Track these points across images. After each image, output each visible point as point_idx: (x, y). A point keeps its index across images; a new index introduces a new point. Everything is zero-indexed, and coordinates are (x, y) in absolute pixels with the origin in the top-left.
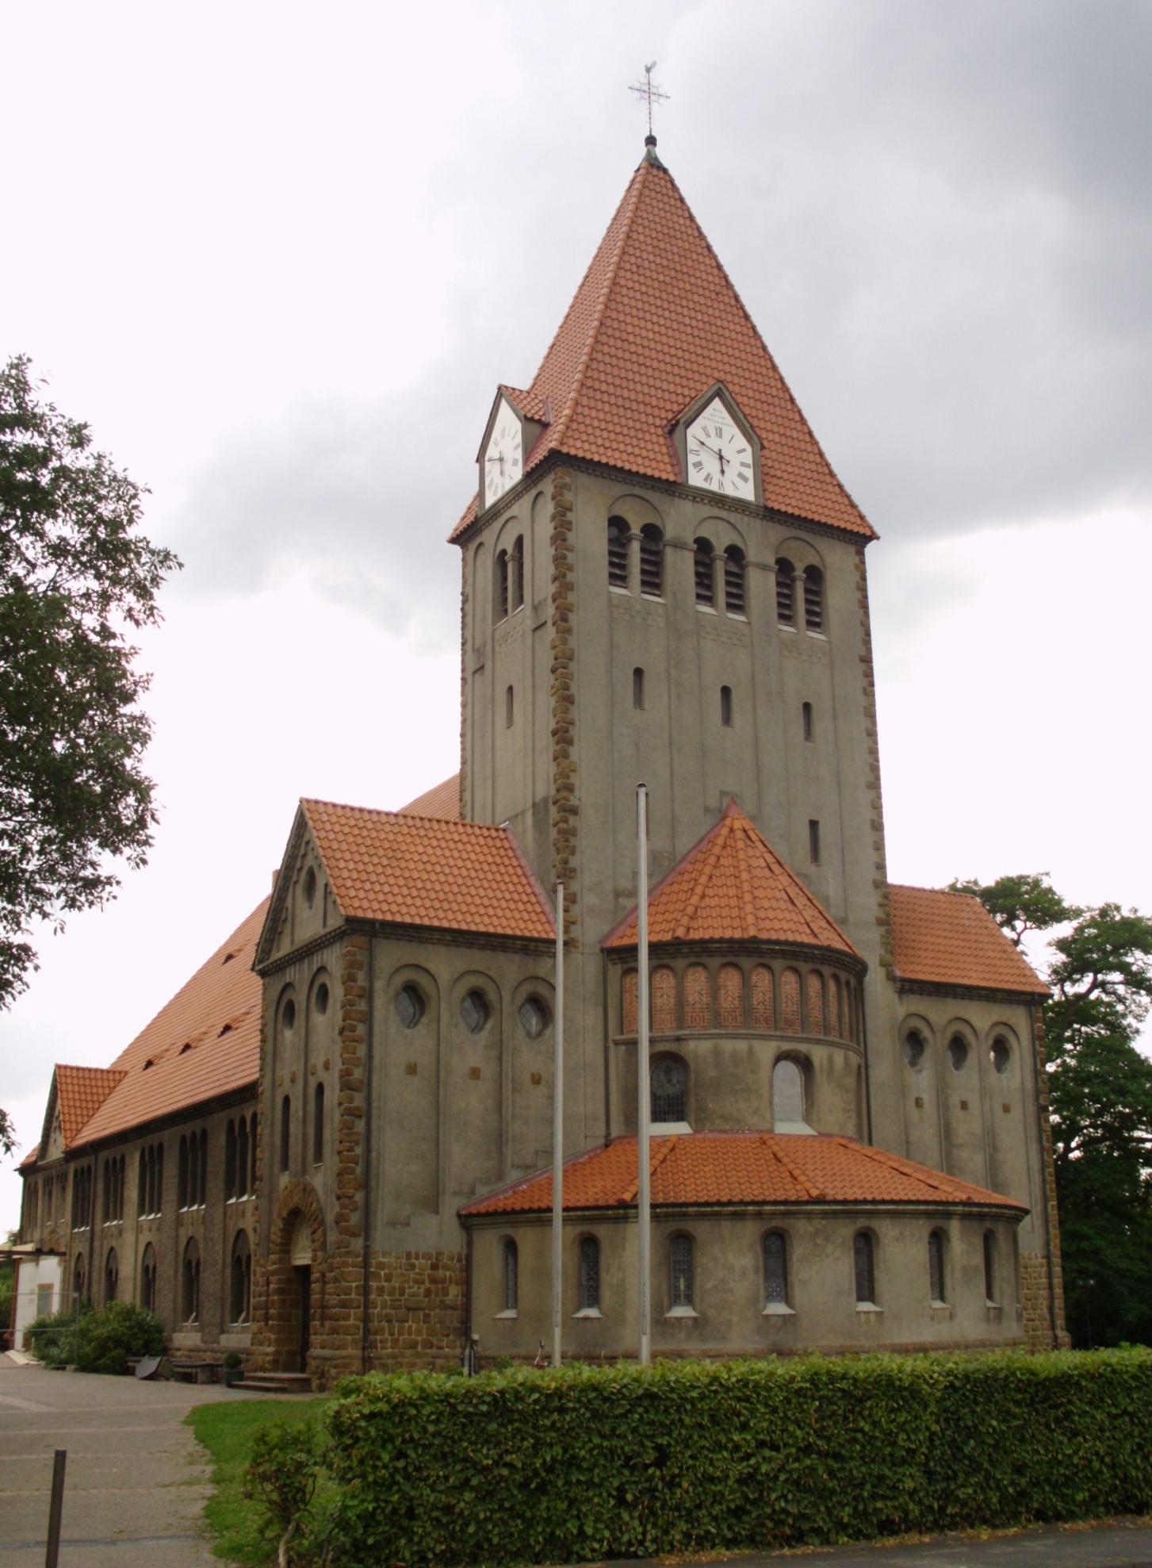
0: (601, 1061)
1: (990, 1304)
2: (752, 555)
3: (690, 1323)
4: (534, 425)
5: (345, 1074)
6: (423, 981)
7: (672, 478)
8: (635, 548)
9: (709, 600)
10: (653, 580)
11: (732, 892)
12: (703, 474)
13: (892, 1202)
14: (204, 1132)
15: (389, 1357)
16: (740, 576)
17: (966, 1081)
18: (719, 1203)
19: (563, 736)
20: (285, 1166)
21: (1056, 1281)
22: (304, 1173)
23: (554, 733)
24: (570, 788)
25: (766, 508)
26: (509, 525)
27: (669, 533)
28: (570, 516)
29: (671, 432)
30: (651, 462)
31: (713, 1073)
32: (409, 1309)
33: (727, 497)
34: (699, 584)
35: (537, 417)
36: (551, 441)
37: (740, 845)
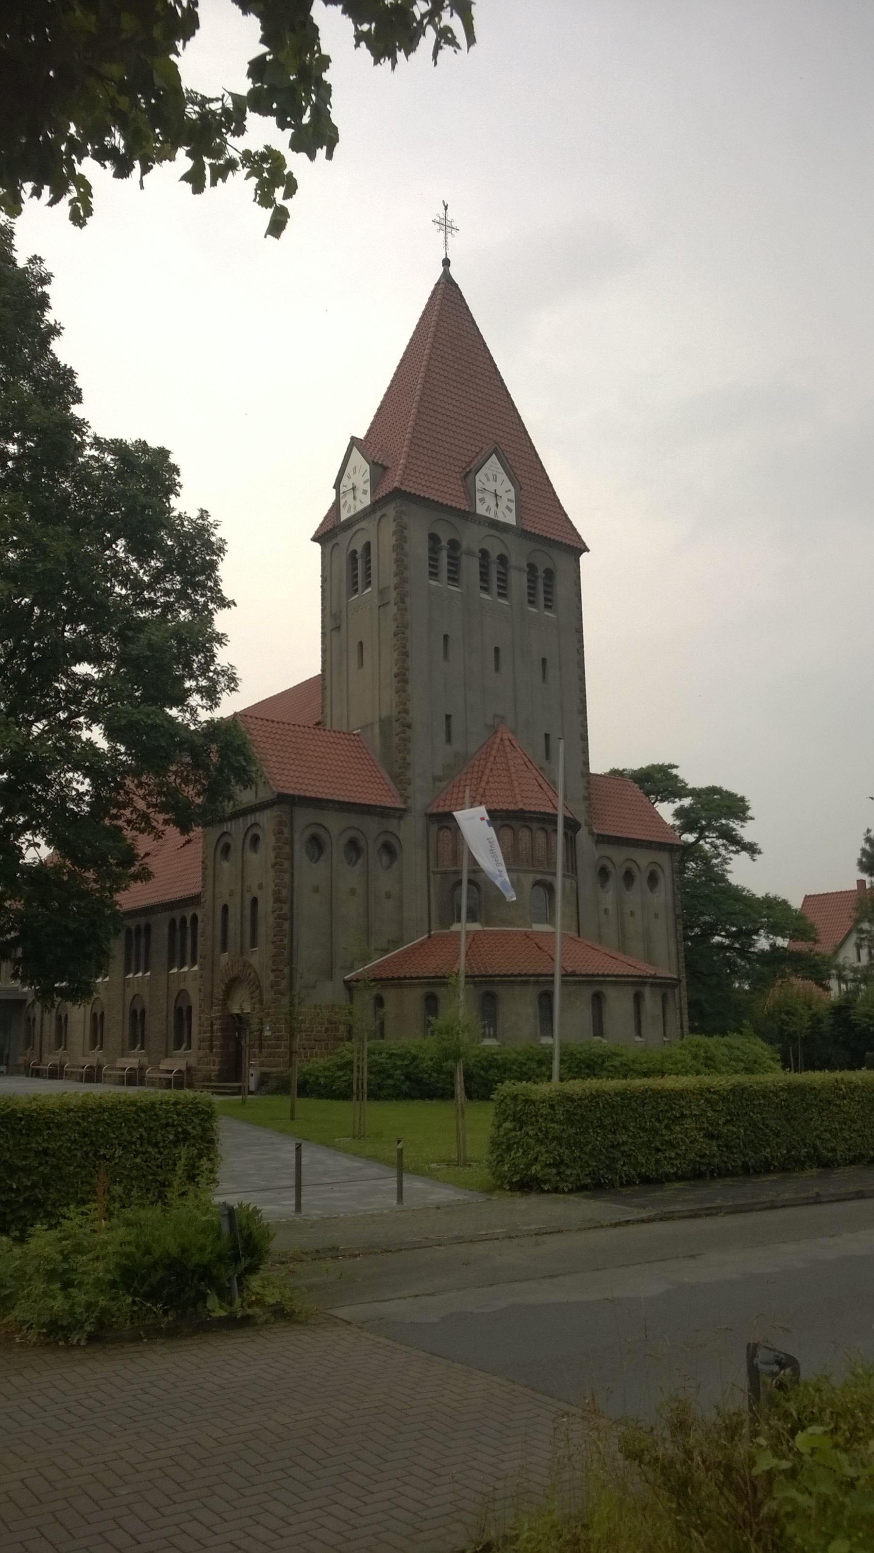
0: (426, 884)
1: (665, 1039)
2: (513, 561)
4: (379, 471)
6: (322, 832)
7: (467, 509)
8: (444, 555)
9: (485, 589)
10: (454, 577)
11: (506, 780)
12: (485, 506)
13: (613, 976)
14: (148, 928)
16: (504, 574)
17: (634, 897)
18: (512, 975)
19: (402, 677)
20: (224, 949)
21: (685, 1023)
22: (242, 954)
23: (396, 676)
24: (406, 711)
26: (359, 534)
27: (464, 545)
28: (406, 532)
29: (465, 477)
32: (316, 1041)
33: (499, 522)
34: (482, 580)
35: (380, 462)
36: (394, 481)
37: (508, 749)
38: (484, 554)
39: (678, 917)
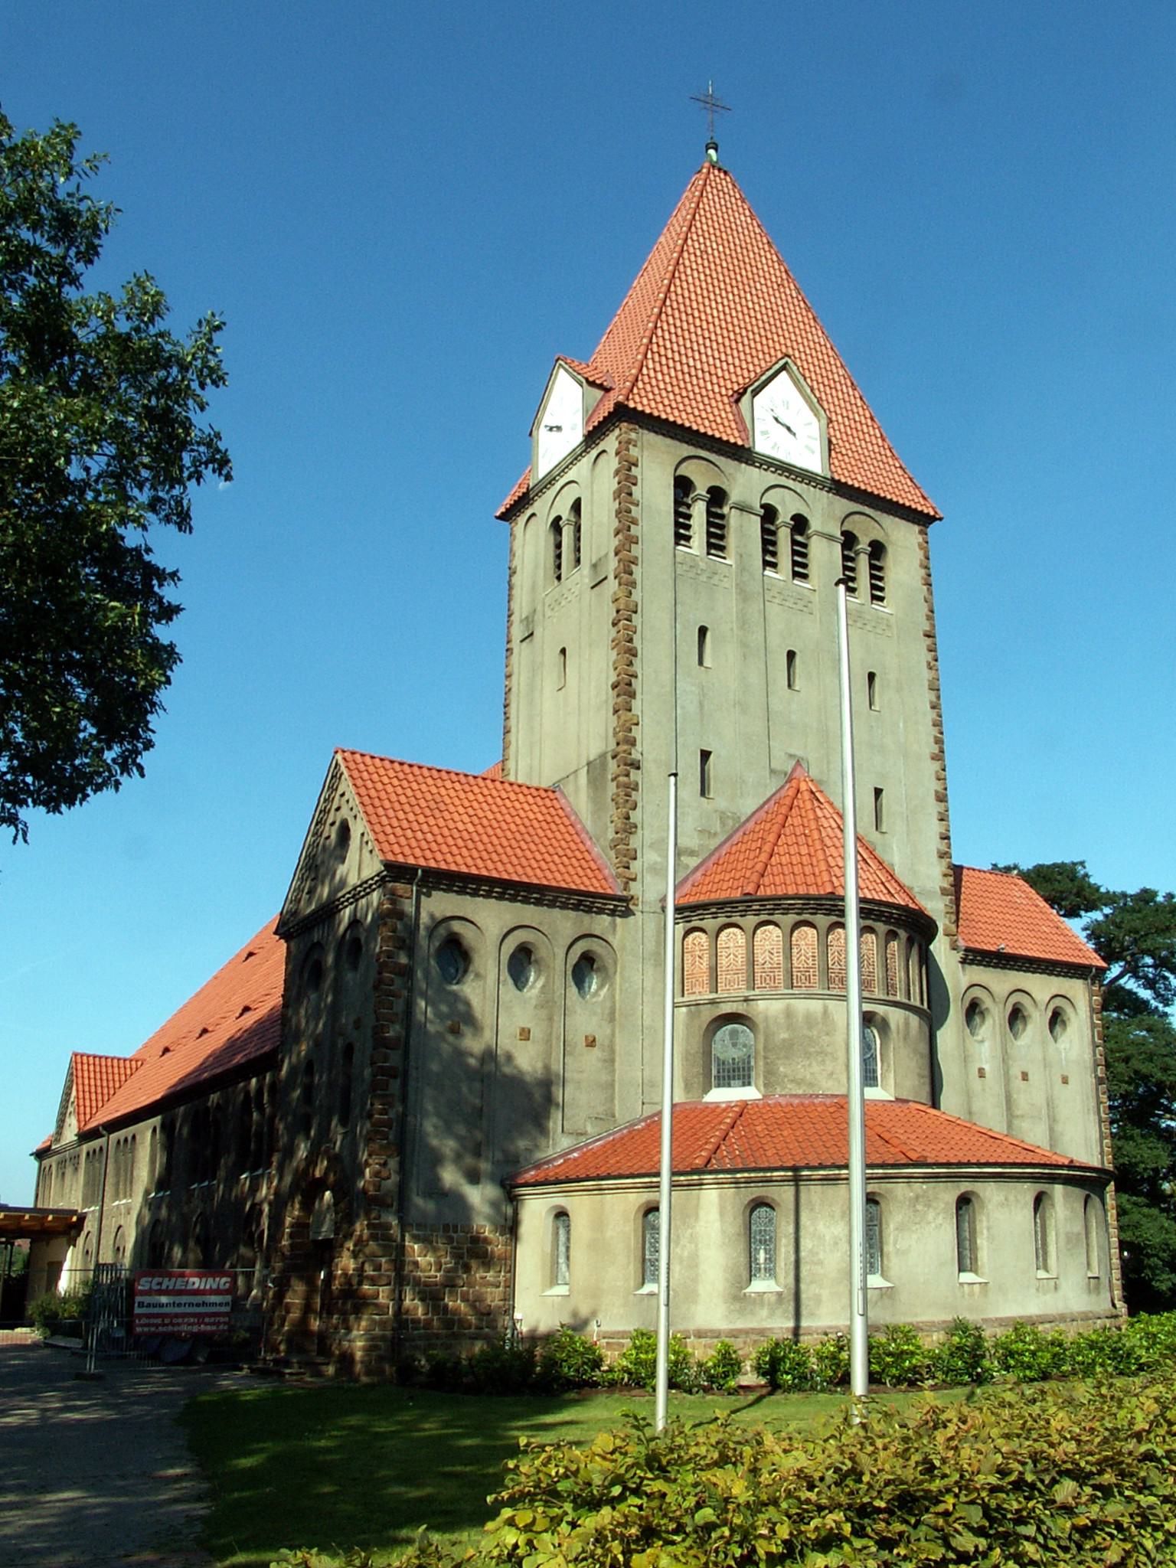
2: (815, 525)
3: (773, 1298)
5: (378, 1030)
7: (740, 443)
10: (716, 542)
15: (420, 1337)
19: (625, 688)
23: (614, 687)
25: (833, 479)
27: (734, 496)
30: (718, 424)
31: (784, 1035)
38: (769, 514)
39: (1100, 1081)
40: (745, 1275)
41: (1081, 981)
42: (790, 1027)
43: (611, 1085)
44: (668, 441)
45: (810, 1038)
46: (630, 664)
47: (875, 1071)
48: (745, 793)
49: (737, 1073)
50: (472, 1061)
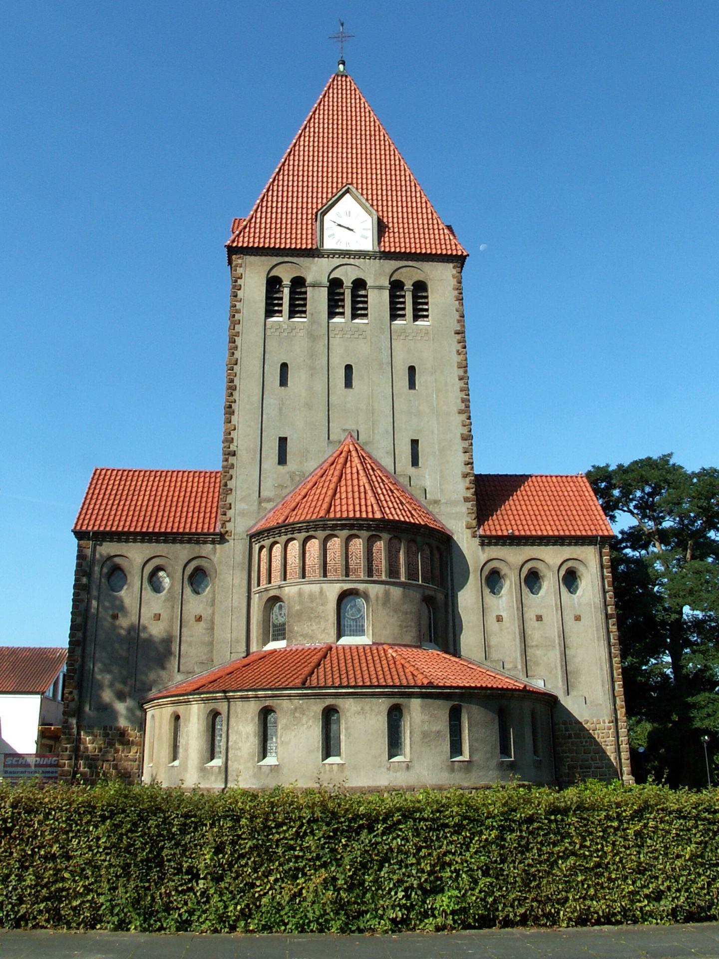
27: (309, 280)
31: (297, 607)
40: (208, 755)
41: (592, 547)
42: (301, 602)
43: (211, 644)
44: (263, 258)
45: (312, 609)
46: (231, 395)
47: (363, 626)
48: (309, 457)
49: (280, 632)
50: (123, 632)
